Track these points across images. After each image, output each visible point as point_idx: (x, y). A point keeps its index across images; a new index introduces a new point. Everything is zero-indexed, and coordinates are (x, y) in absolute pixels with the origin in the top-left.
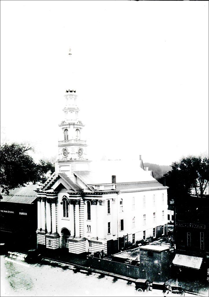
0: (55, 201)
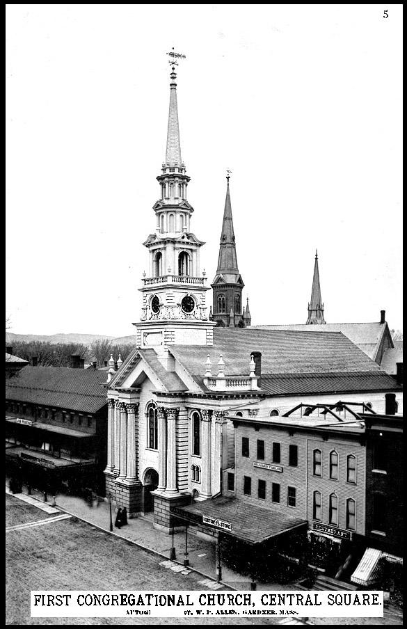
0: (136, 408)
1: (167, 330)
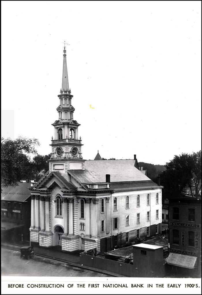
1: (67, 163)
